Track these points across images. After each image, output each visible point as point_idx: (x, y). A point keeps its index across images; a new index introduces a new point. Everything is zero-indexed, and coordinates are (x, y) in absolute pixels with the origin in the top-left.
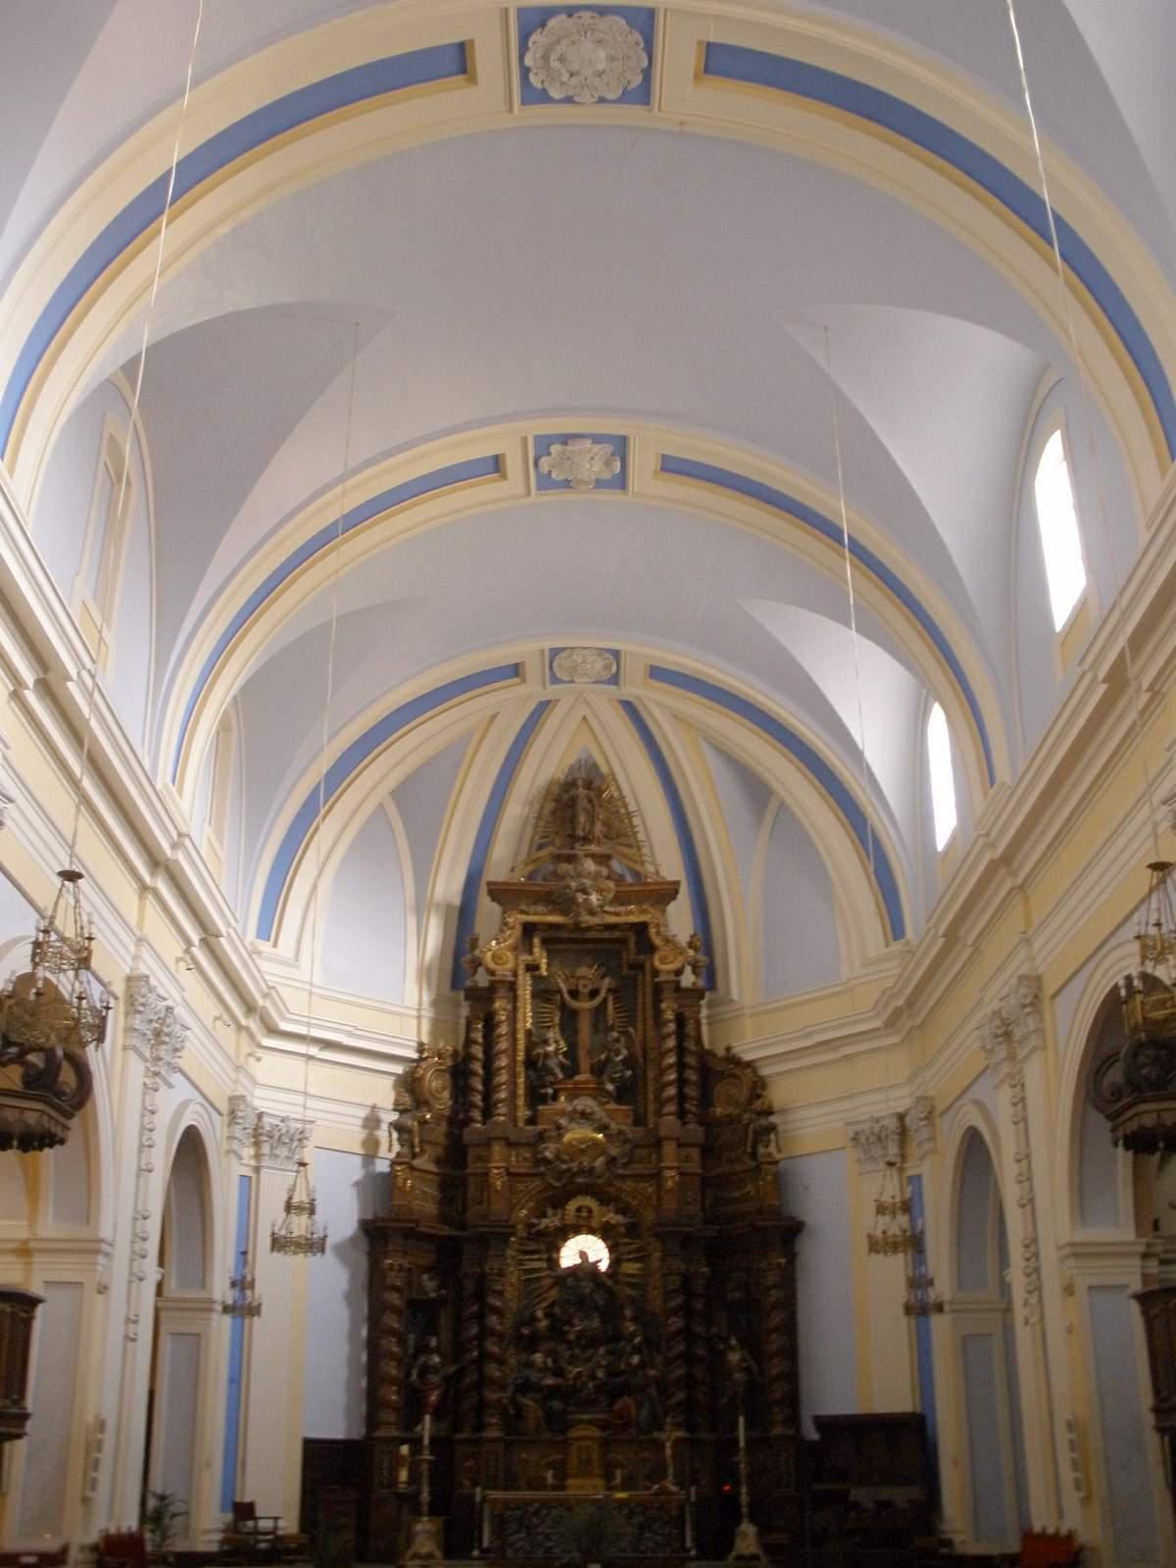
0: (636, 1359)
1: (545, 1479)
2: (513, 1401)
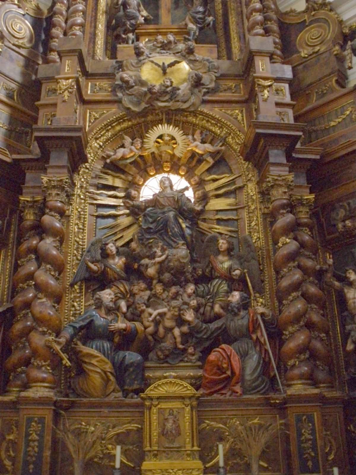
0: (236, 296)
1: (112, 458)
2: (68, 348)
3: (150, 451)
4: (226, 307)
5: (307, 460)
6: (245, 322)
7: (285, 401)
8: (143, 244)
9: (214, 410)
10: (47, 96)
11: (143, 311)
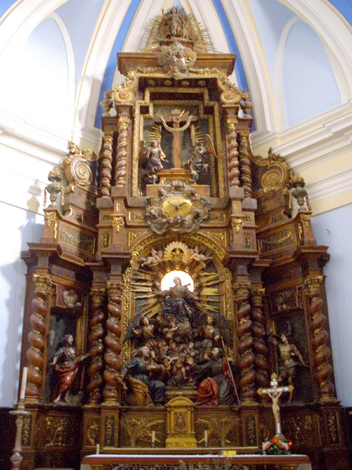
0: (216, 351)
1: (150, 438)
2: (126, 380)
3: (170, 434)
4: (211, 355)
5: (250, 440)
6: (221, 365)
7: (241, 409)
8: (164, 318)
9: (143, 299)
10: (103, 220)
11: (164, 358)
